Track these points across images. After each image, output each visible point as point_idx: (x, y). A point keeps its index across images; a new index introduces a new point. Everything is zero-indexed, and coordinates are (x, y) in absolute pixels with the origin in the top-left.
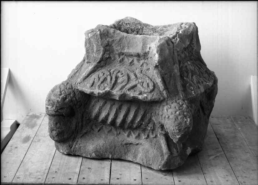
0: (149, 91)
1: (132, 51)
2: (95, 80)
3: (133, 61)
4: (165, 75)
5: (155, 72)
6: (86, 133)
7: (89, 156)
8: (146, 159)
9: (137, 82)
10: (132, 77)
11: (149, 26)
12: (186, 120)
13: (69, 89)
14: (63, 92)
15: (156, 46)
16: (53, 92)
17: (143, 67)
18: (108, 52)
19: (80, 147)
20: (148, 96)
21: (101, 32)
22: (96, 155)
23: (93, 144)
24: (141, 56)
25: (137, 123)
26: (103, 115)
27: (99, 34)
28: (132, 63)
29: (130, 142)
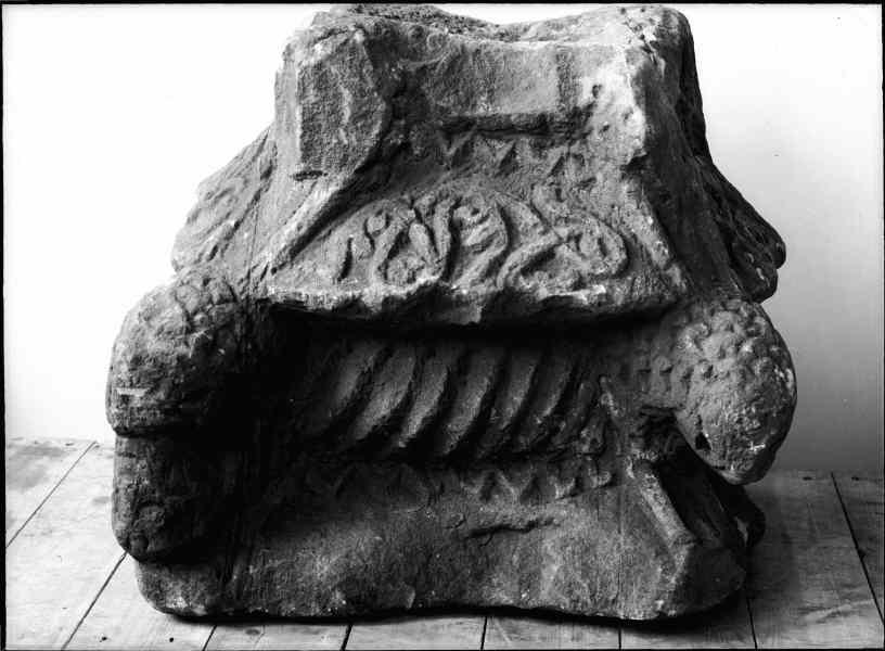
0: (614, 272)
1: (513, 107)
2: (354, 246)
3: (512, 153)
4: (664, 201)
5: (625, 187)
7: (315, 610)
8: (588, 581)
9: (551, 239)
10: (526, 218)
11: (483, 26)
12: (782, 375)
13: (223, 300)
14: (198, 317)
15: (625, 75)
16: (148, 319)
17: (560, 177)
18: (403, 122)
19: (271, 572)
20: (614, 291)
21: (366, 33)
22: (348, 600)
23: (327, 553)
24: (551, 128)
25: (540, 426)
26: (382, 406)
27: (364, 43)
28: (508, 165)
29: (498, 521)
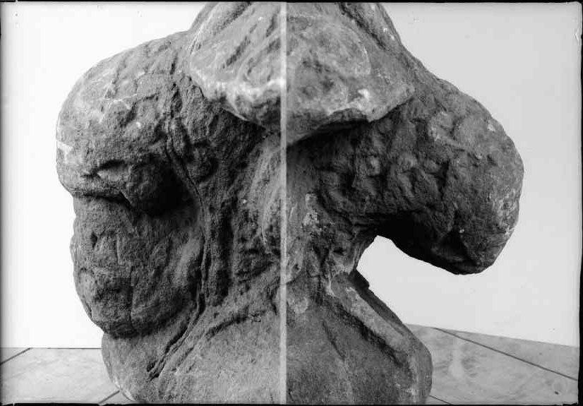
6: (239, 319)
14: (126, 82)
